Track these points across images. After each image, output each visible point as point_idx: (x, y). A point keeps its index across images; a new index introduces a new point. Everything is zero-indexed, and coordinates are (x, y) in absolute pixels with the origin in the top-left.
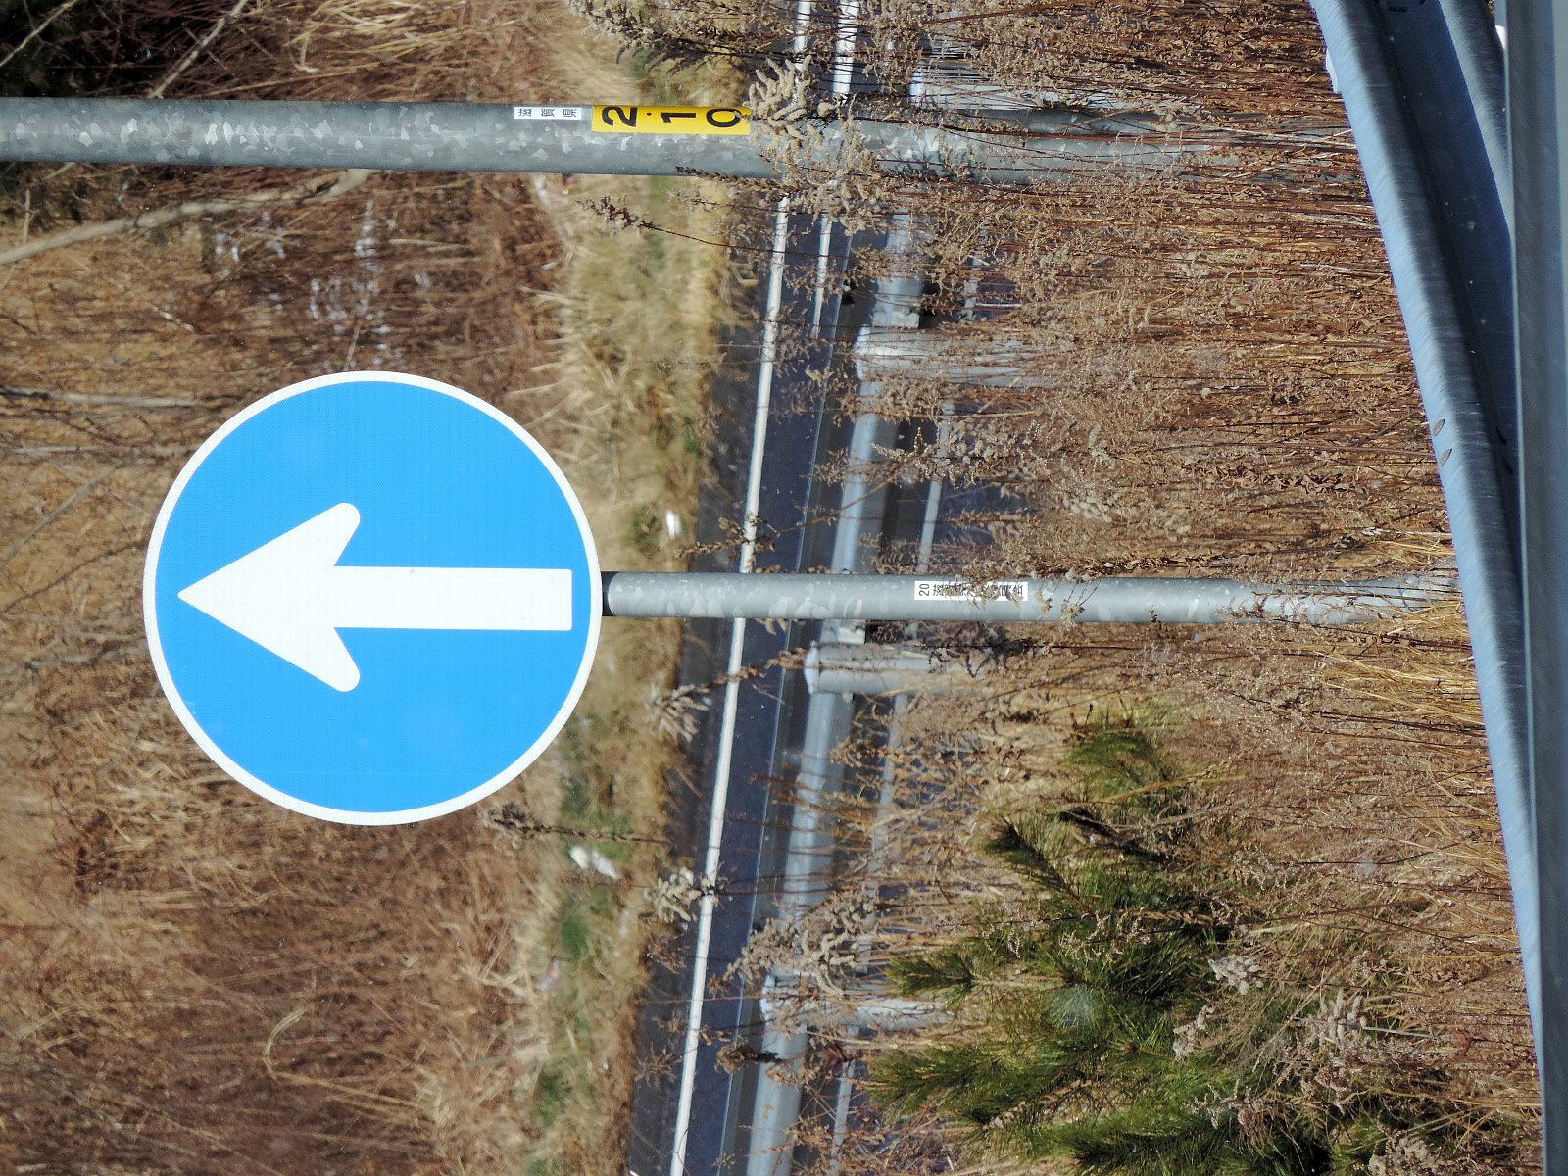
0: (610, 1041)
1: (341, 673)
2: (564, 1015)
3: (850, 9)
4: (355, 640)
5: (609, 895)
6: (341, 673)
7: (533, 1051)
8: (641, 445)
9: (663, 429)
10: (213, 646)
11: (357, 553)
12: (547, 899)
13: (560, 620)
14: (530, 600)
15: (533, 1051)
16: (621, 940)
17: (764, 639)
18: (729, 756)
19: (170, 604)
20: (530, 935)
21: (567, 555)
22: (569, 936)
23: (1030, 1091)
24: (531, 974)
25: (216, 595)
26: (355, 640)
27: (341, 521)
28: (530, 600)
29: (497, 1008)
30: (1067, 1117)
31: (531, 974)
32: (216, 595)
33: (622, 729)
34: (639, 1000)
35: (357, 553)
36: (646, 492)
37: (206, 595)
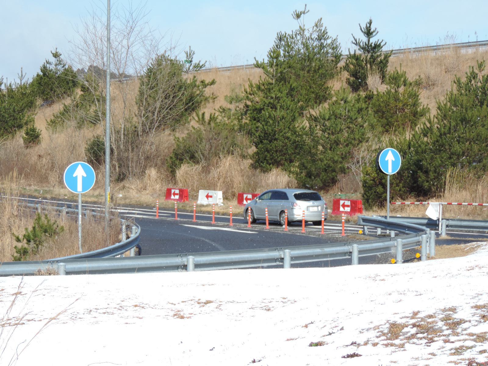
0: (29, 193)
1: (74, 175)
2: (30, 190)
3: (486, 230)
4: (76, 177)
5: (39, 193)
6: (74, 175)
7: (28, 188)
8: (72, 195)
9: (73, 197)
10: (77, 166)
11: (83, 177)
12: (38, 189)
13: (78, 190)
14: (80, 188)
15: (28, 188)
16: (36, 194)
17: (82, 203)
18: (71, 202)
19: (80, 163)
20: (36, 188)
21: (83, 191)
22: (36, 190)
23: (38, 223)
24: (33, 187)
25: (80, 167)
26: (76, 177)
27: (85, 175)
28: (80, 188)
29: (30, 185)
30: (37, 226)
31: (33, 187)
32: (80, 167)
33: (401, 209)
34: (32, 195)
35: (83, 177)
36: (68, 196)
37: (80, 166)
